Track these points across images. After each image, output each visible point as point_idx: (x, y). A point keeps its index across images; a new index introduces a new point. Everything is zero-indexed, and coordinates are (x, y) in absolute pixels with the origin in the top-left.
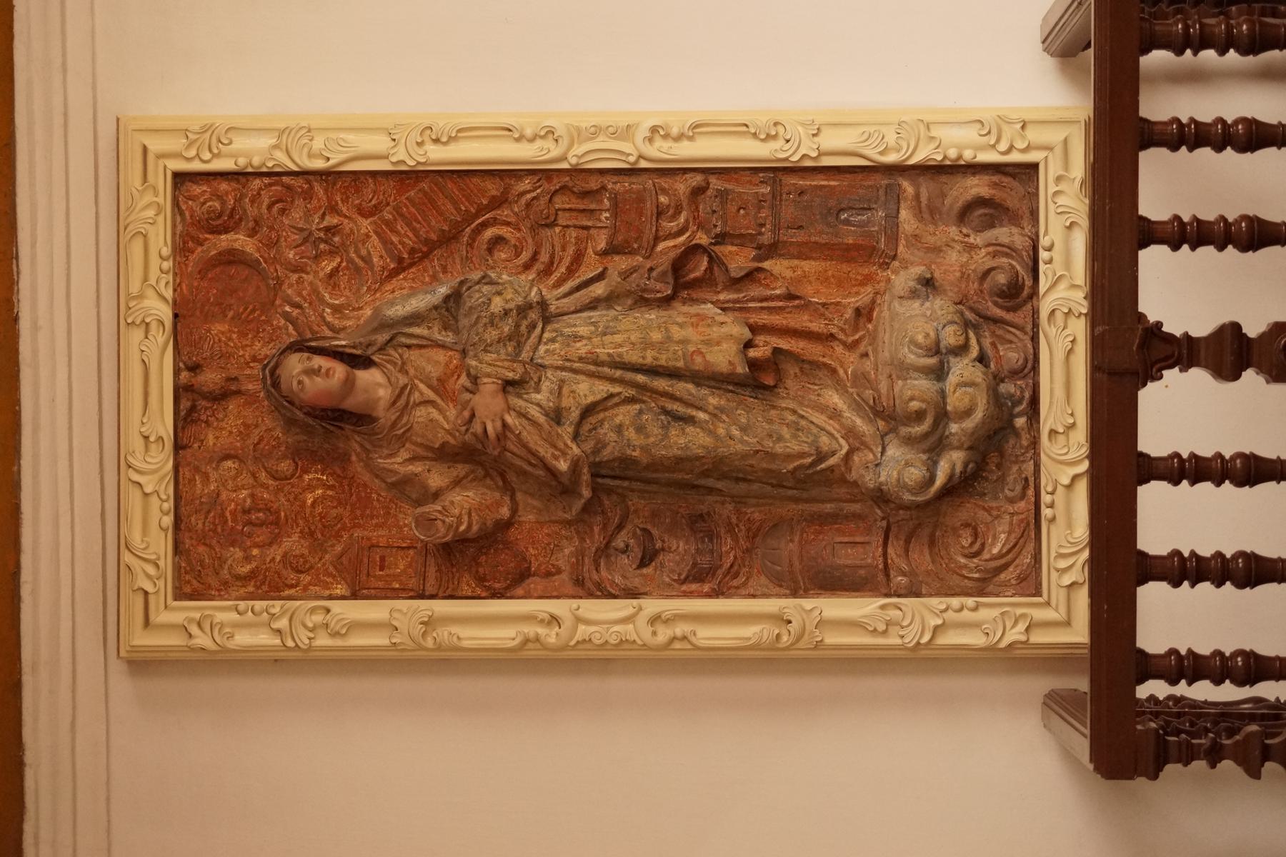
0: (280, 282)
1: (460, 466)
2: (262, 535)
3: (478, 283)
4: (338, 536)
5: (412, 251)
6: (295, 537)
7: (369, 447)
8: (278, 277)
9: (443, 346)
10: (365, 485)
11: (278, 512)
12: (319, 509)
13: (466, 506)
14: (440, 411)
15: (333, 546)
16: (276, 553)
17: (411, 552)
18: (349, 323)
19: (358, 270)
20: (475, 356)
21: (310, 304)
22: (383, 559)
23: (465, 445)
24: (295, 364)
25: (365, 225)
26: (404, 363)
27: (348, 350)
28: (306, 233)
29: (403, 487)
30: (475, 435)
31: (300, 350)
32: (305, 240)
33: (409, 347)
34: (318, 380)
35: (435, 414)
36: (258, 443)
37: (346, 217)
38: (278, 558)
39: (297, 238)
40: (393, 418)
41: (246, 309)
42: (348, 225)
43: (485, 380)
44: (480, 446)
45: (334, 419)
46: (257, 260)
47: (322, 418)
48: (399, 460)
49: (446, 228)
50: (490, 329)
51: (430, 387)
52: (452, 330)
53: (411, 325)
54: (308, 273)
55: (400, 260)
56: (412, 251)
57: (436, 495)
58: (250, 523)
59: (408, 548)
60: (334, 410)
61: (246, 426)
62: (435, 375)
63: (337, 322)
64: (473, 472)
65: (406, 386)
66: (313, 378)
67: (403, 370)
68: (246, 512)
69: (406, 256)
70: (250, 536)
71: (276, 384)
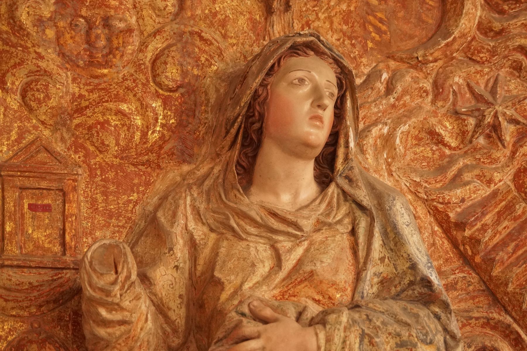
0: (419, 65)
1: (183, 312)
2: (75, 44)
3: (446, 330)
4: (77, 147)
5: (475, 241)
6: (74, 89)
7: (205, 187)
8: (426, 63)
9: (358, 278)
10: (148, 184)
11: (107, 64)
12: (114, 121)
13: (135, 317)
14: (267, 278)
15: (63, 139)
16: (51, 61)
17: (57, 248)
18: (370, 159)
19: (442, 169)
20: (354, 321)
21: (393, 106)
22: (47, 208)
23: (220, 314)
24: (325, 76)
25: (504, 179)
26: (330, 225)
27: (341, 152)
28: (491, 99)
29: (152, 232)
30: (238, 325)
31: (340, 86)
32: (478, 97)
33: (353, 232)
34: (307, 106)
35: (263, 269)
36: (202, 38)
37: (514, 153)
38: (43, 64)
39: (481, 88)
40: (253, 214)
41: (381, 21)
42: (501, 154)
43: (322, 336)
44: (220, 334)
45: (245, 137)
46: (448, 34)
47: (248, 117)
48: (192, 225)
49: (511, 288)
50: (392, 342)
51: (300, 262)
52: (380, 291)
53: (385, 234)
54: (433, 102)
55: (461, 226)
56: (475, 241)
57: (145, 279)
58: (90, 27)
59: (63, 244)
60: (260, 132)
61: (223, 24)
62: (319, 267)
63: (371, 141)
64: (175, 331)
65: (299, 228)
66: (304, 104)
67: (320, 225)
68: (107, 22)
69: (467, 233)
70: (73, 26)
71: (296, 50)
